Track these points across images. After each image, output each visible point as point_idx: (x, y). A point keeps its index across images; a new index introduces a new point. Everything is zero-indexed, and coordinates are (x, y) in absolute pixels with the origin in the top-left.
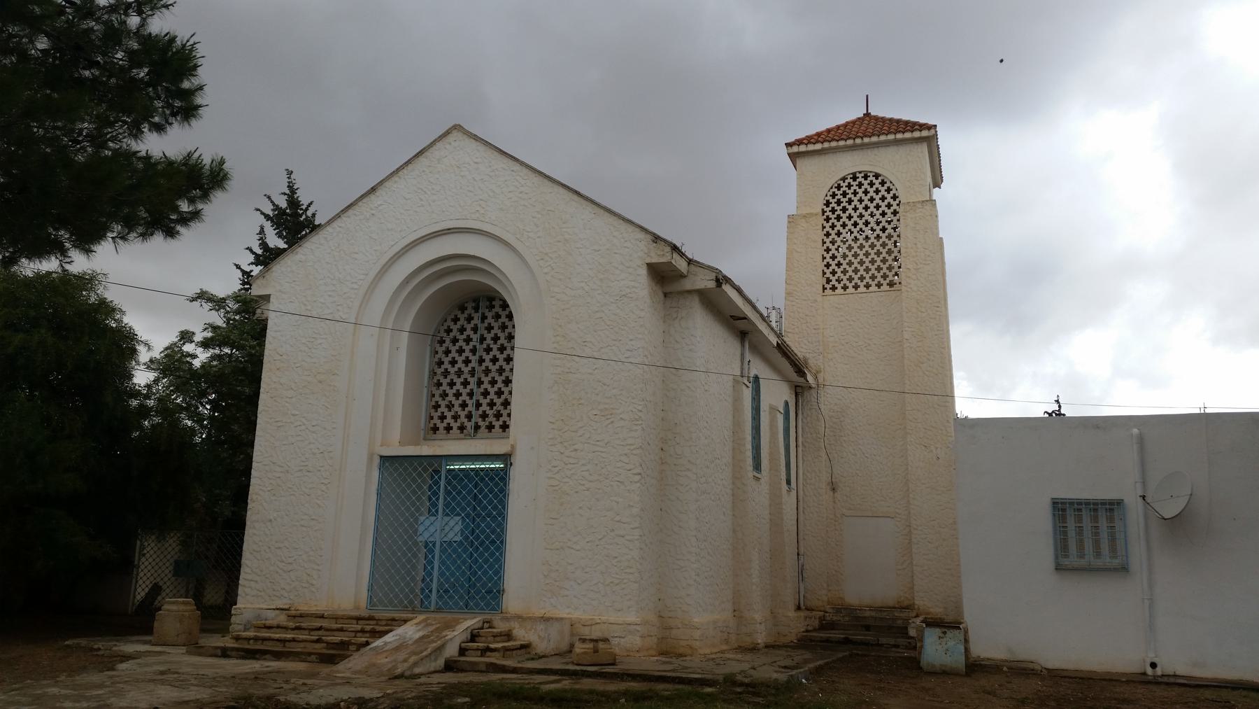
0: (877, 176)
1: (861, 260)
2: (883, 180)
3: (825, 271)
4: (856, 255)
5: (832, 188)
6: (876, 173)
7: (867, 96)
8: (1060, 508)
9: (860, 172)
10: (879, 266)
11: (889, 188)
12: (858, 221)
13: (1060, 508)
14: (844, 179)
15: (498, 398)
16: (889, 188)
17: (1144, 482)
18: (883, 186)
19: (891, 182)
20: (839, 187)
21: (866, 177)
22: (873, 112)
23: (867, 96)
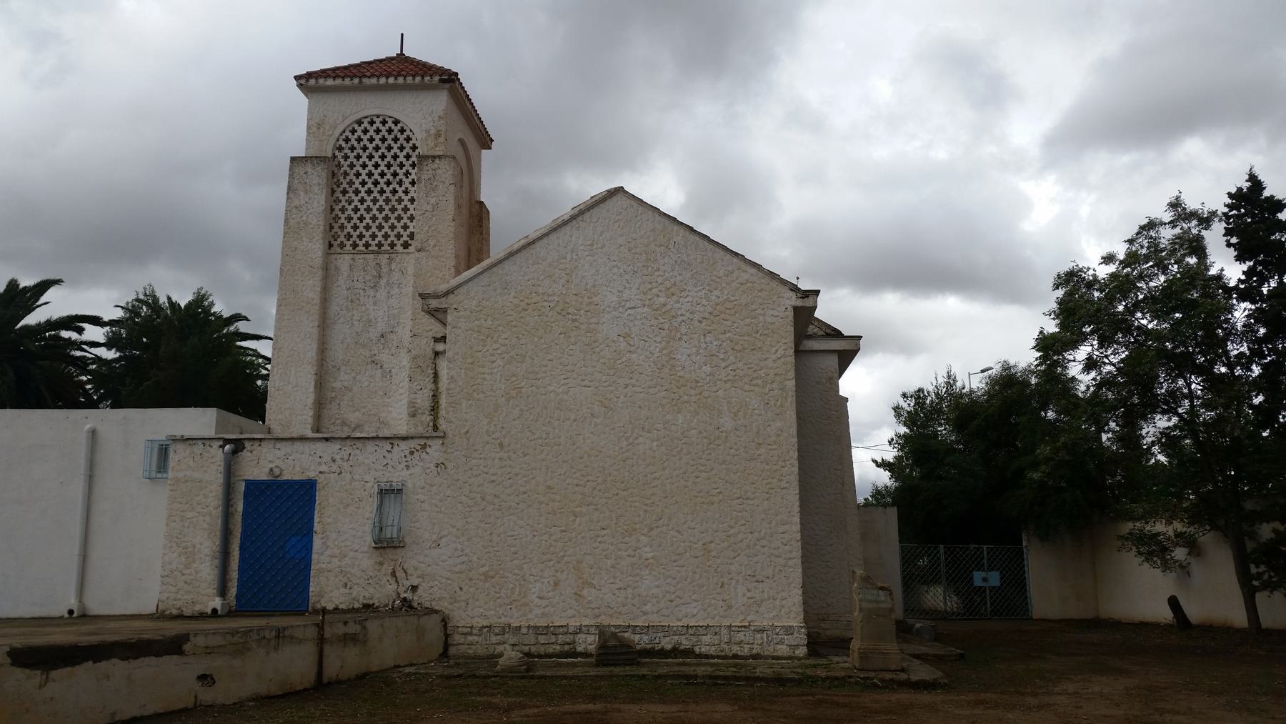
0: (396, 122)
1: (386, 233)
2: (402, 128)
3: (333, 225)
4: (374, 219)
5: (344, 132)
6: (395, 119)
7: (402, 35)
8: (291, 158)
9: (378, 116)
10: (367, 242)
11: (408, 136)
12: (373, 169)
13: (291, 158)
14: (360, 122)
15: (375, 215)
16: (408, 136)
17: (436, 374)
18: (363, 186)
19: (411, 131)
20: (347, 140)
21: (384, 123)
22: (407, 53)
23: (402, 35)
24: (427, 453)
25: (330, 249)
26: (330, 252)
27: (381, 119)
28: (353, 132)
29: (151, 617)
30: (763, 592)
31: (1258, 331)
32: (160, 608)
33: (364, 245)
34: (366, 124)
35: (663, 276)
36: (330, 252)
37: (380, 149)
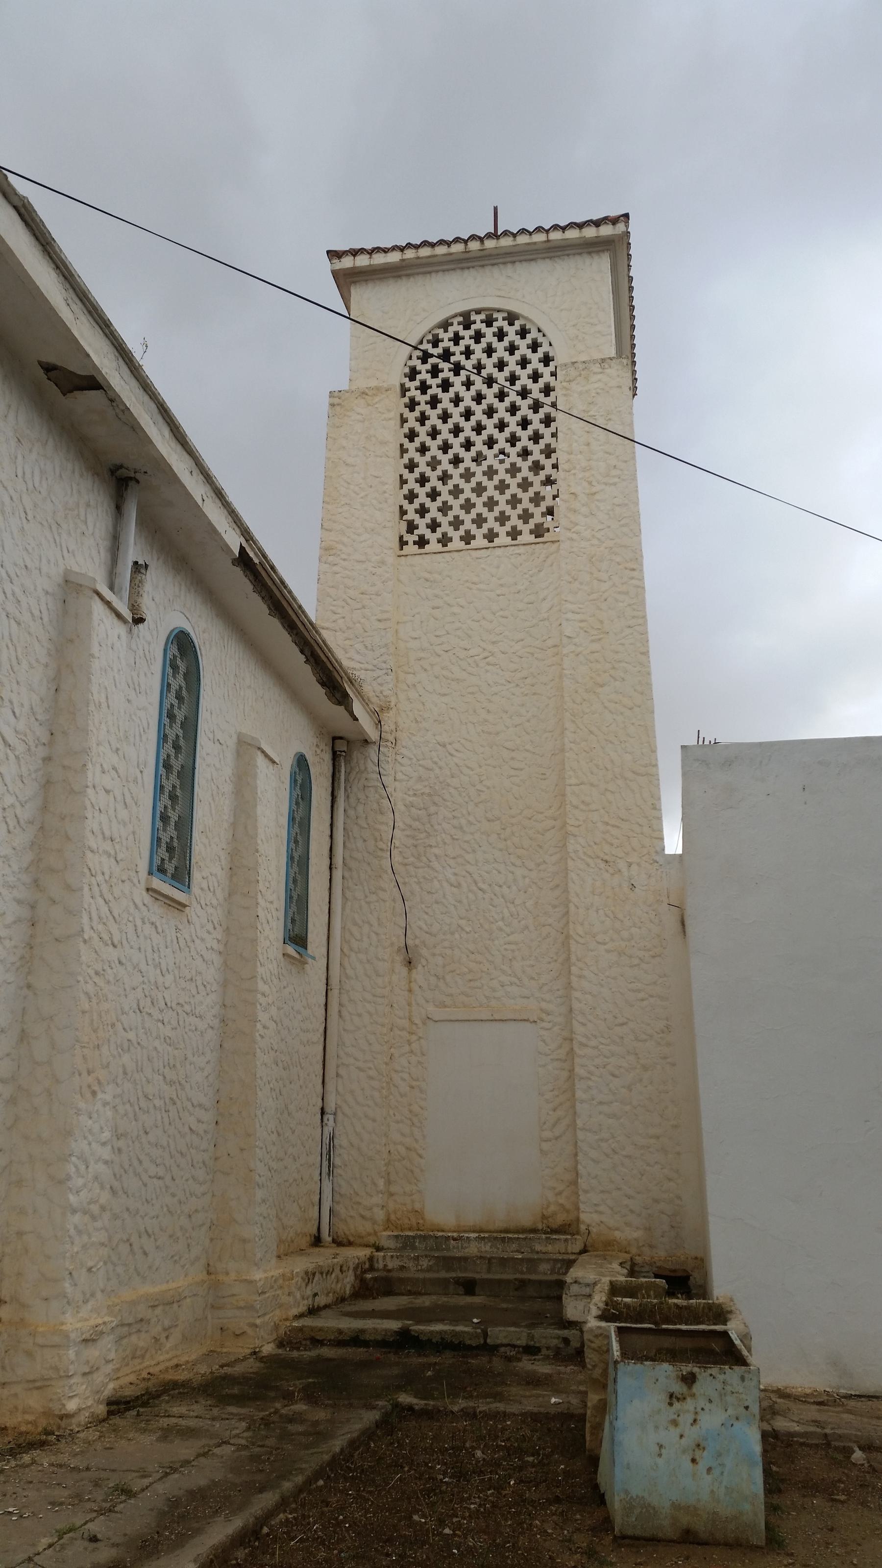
0: (511, 318)
7: (496, 209)
9: (478, 312)
19: (539, 331)
21: (489, 323)
23: (496, 209)
24: (9, 866)
25: (402, 549)
26: (402, 553)
27: (483, 316)
28: (435, 343)
29: (232, 515)
30: (265, 1027)
31: (491, 1247)
32: (310, 960)
33: (462, 538)
34: (456, 327)
35: (608, 1058)
36: (402, 553)
37: (429, 481)
